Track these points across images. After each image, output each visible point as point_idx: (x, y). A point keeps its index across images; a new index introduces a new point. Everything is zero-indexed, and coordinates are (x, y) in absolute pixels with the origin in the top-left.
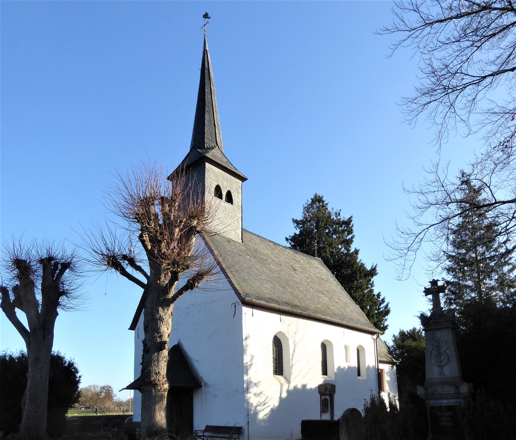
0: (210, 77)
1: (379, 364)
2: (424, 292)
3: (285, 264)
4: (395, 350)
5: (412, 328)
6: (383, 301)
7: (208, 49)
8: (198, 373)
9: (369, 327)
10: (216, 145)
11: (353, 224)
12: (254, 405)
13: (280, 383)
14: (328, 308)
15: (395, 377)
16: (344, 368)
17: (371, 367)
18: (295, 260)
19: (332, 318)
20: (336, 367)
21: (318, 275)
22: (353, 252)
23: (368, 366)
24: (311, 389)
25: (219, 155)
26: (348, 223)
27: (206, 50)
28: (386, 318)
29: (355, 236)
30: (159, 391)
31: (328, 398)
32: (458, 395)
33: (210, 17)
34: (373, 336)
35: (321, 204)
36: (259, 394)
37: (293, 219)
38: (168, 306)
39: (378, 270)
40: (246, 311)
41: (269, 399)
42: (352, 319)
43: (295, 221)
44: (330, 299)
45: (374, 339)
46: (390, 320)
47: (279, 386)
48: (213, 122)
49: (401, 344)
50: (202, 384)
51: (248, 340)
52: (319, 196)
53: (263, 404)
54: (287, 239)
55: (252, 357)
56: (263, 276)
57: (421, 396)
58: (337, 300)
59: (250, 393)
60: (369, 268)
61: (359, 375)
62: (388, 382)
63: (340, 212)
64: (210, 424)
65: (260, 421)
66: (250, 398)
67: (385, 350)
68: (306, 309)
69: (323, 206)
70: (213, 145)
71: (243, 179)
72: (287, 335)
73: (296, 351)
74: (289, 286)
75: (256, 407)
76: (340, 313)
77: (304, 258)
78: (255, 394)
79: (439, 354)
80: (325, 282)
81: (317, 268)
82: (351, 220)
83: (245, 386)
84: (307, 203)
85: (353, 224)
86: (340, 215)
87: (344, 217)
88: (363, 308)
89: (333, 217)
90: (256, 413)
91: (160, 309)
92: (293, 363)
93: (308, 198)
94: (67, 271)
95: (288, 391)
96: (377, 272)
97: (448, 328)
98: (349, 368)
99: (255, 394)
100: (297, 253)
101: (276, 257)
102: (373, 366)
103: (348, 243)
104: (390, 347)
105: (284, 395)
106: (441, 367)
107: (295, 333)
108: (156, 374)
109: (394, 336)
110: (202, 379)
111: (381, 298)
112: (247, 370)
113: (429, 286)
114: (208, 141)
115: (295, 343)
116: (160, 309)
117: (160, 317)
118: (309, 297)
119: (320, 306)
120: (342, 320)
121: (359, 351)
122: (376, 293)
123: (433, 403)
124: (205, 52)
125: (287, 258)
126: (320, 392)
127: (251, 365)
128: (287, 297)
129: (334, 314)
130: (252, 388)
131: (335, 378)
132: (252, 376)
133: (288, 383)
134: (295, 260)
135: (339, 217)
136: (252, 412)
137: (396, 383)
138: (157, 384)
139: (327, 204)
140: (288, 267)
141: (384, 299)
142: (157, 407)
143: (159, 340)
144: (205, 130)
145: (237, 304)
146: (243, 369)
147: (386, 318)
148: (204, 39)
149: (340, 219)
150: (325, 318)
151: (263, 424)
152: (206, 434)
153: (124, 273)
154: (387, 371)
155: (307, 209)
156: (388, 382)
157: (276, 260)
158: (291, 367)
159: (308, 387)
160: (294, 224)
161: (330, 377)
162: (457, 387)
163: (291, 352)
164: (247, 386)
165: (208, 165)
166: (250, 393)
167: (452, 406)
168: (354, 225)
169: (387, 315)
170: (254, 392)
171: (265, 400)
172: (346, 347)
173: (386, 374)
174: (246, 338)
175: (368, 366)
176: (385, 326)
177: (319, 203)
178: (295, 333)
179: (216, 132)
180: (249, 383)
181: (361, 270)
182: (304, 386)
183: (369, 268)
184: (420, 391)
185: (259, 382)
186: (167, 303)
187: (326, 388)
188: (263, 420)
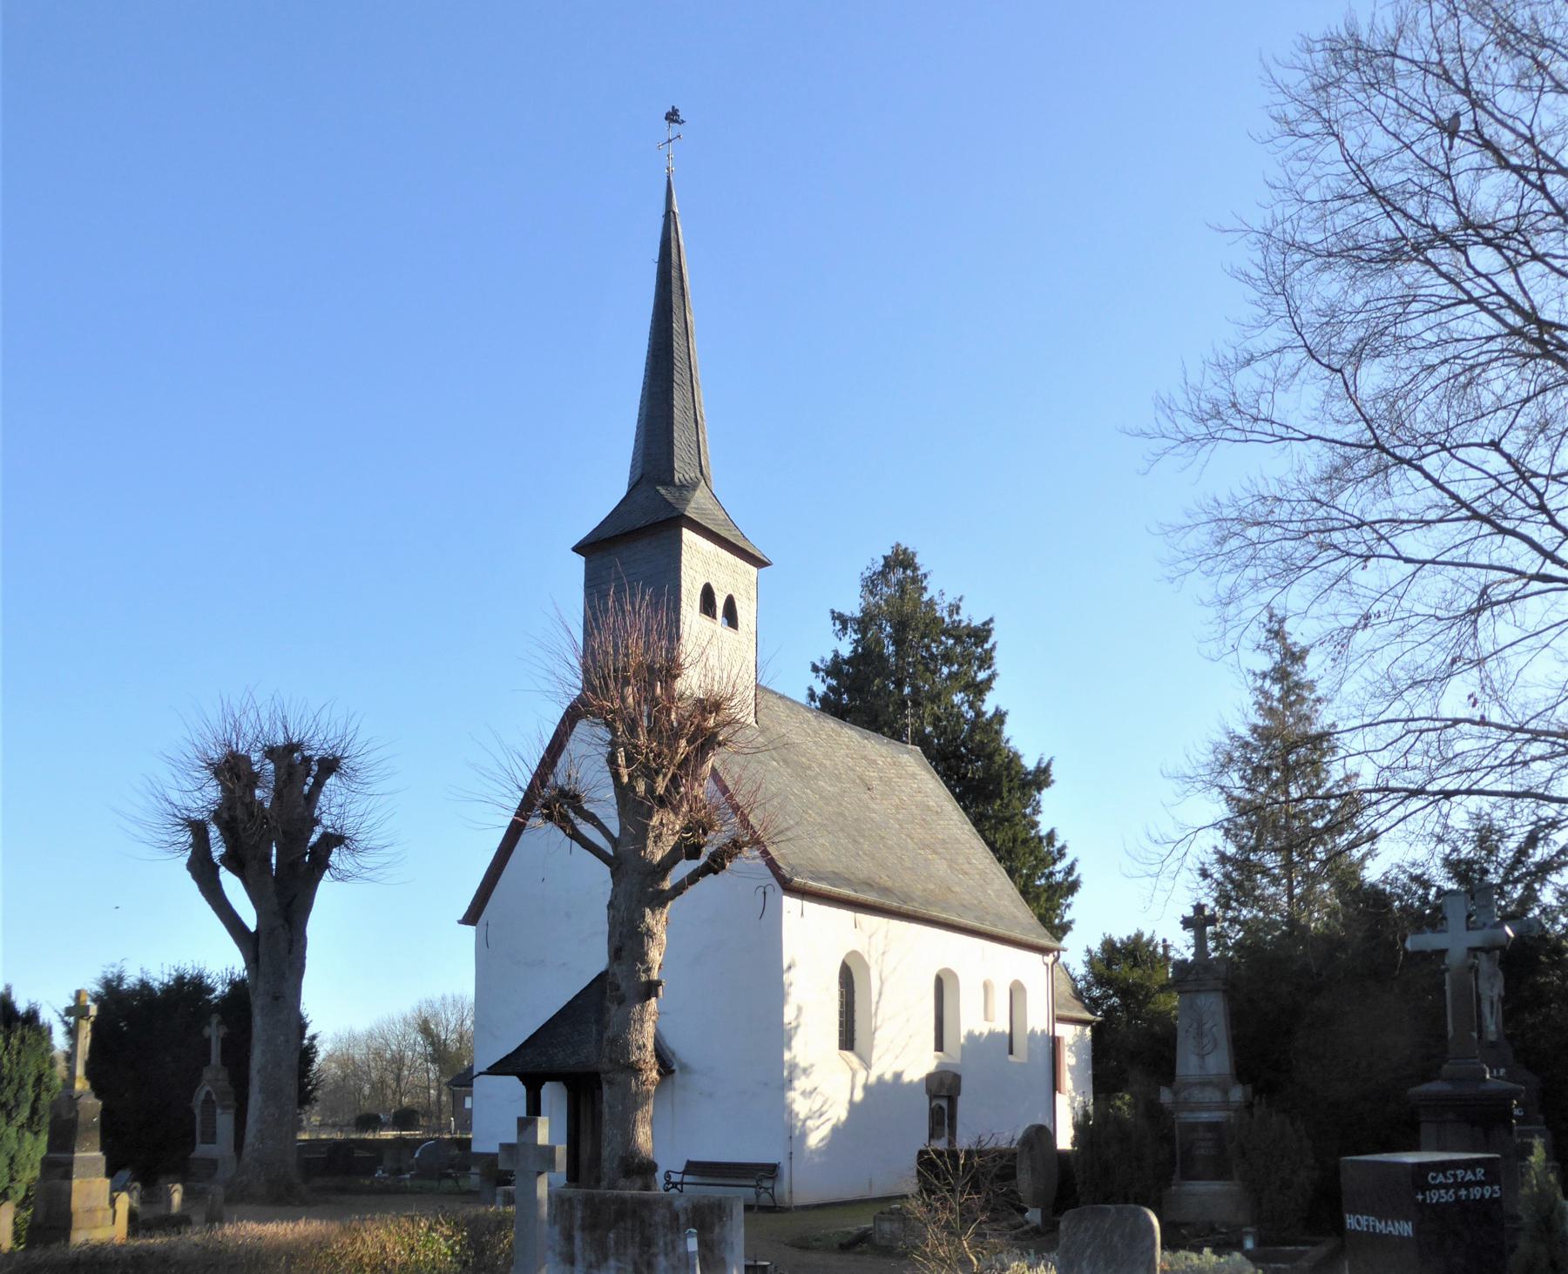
0: (683, 289)
1: (1056, 1025)
2: (1182, 922)
3: (847, 774)
4: (1089, 989)
5: (1132, 933)
6: (1061, 853)
7: (677, 211)
8: (664, 1041)
9: (1039, 936)
10: (699, 475)
11: (995, 643)
12: (802, 1116)
13: (852, 1069)
14: (950, 889)
15: (1087, 1056)
16: (981, 1034)
17: (1039, 1033)
18: (864, 758)
19: (961, 917)
20: (964, 1032)
21: (919, 798)
22: (991, 718)
23: (1032, 1031)
24: (911, 1082)
25: (709, 505)
26: (981, 634)
27: (674, 213)
28: (1068, 902)
29: (997, 675)
30: (643, 1083)
31: (944, 1104)
32: (1225, 1105)
33: (683, 122)
34: (1045, 958)
35: (909, 572)
36: (811, 1093)
37: (833, 612)
38: (663, 905)
39: (1055, 772)
40: (790, 904)
41: (829, 1103)
42: (999, 917)
43: (841, 620)
44: (952, 863)
45: (1047, 965)
46: (1077, 909)
47: (849, 1074)
48: (692, 412)
49: (1106, 973)
50: (675, 1067)
51: (793, 971)
52: (906, 549)
53: (818, 1114)
54: (815, 669)
55: (800, 1009)
56: (810, 816)
57: (1166, 1106)
58: (966, 867)
59: (794, 1090)
60: (1029, 763)
61: (1011, 1052)
62: (1071, 1069)
63: (961, 604)
64: (694, 1158)
65: (812, 1152)
66: (794, 1101)
67: (1065, 989)
68: (908, 898)
69: (915, 580)
70: (693, 475)
71: (758, 562)
72: (866, 958)
73: (883, 997)
74: (863, 836)
75: (805, 1121)
76: (976, 902)
77: (884, 750)
78: (803, 1093)
79: (1200, 1034)
80: (935, 818)
81: (913, 776)
82: (989, 631)
83: (785, 1073)
84: (870, 566)
85: (995, 643)
86: (960, 612)
87: (971, 615)
88: (1011, 872)
89: (942, 612)
90: (804, 1135)
91: (648, 911)
92: (878, 1024)
93: (874, 555)
94: (332, 781)
95: (866, 1088)
96: (1052, 778)
97: (1216, 990)
98: (992, 1034)
99: (803, 1093)
100: (866, 739)
101: (826, 755)
102: (1043, 1031)
103: (979, 690)
104: (1079, 978)
105: (859, 1095)
106: (1202, 1057)
107: (884, 953)
108: (639, 1048)
109: (1089, 951)
110: (674, 1054)
111: (1058, 844)
112: (790, 1039)
113: (1190, 913)
114: (682, 465)
115: (883, 977)
116: (648, 911)
117: (648, 929)
118: (908, 864)
119: (931, 886)
120: (982, 920)
121: (1016, 993)
122: (1044, 830)
123: (1188, 1117)
124: (669, 215)
125: (847, 756)
126: (929, 1091)
127: (797, 1027)
128: (864, 868)
129: (963, 906)
130: (799, 1078)
131: (962, 1059)
132: (799, 1051)
133: (866, 1069)
134: (864, 758)
135: (956, 618)
136: (797, 1132)
137: (1090, 1072)
138: (641, 1070)
139: (925, 576)
140: (854, 782)
141: (1064, 847)
142: (640, 1115)
143: (644, 978)
144: (675, 435)
145: (769, 890)
146: (780, 1036)
147: (1068, 902)
148: (666, 179)
149: (960, 621)
150: (946, 919)
151: (817, 1160)
152: (687, 1179)
153: (576, 836)
154: (1071, 1042)
155: (871, 584)
156: (1071, 1069)
157: (828, 763)
158: (874, 1033)
159: (906, 1078)
160: (834, 625)
161: (948, 1055)
162: (1226, 1092)
163: (875, 997)
164: (790, 1073)
165: (687, 535)
166: (794, 1090)
167: (1217, 1122)
168: (997, 646)
169: (1072, 895)
170: (802, 1089)
171: (822, 1106)
172: (987, 987)
173: (1067, 1049)
174: (790, 968)
175: (1032, 1031)
176: (1066, 923)
177: (905, 569)
178: (884, 953)
179: (698, 441)
180: (794, 1067)
181: (1013, 773)
182: (898, 1076)
183: (1029, 763)
184: (1166, 1096)
185: (812, 1066)
186: (660, 900)
187: (941, 1084)
188: (817, 1151)
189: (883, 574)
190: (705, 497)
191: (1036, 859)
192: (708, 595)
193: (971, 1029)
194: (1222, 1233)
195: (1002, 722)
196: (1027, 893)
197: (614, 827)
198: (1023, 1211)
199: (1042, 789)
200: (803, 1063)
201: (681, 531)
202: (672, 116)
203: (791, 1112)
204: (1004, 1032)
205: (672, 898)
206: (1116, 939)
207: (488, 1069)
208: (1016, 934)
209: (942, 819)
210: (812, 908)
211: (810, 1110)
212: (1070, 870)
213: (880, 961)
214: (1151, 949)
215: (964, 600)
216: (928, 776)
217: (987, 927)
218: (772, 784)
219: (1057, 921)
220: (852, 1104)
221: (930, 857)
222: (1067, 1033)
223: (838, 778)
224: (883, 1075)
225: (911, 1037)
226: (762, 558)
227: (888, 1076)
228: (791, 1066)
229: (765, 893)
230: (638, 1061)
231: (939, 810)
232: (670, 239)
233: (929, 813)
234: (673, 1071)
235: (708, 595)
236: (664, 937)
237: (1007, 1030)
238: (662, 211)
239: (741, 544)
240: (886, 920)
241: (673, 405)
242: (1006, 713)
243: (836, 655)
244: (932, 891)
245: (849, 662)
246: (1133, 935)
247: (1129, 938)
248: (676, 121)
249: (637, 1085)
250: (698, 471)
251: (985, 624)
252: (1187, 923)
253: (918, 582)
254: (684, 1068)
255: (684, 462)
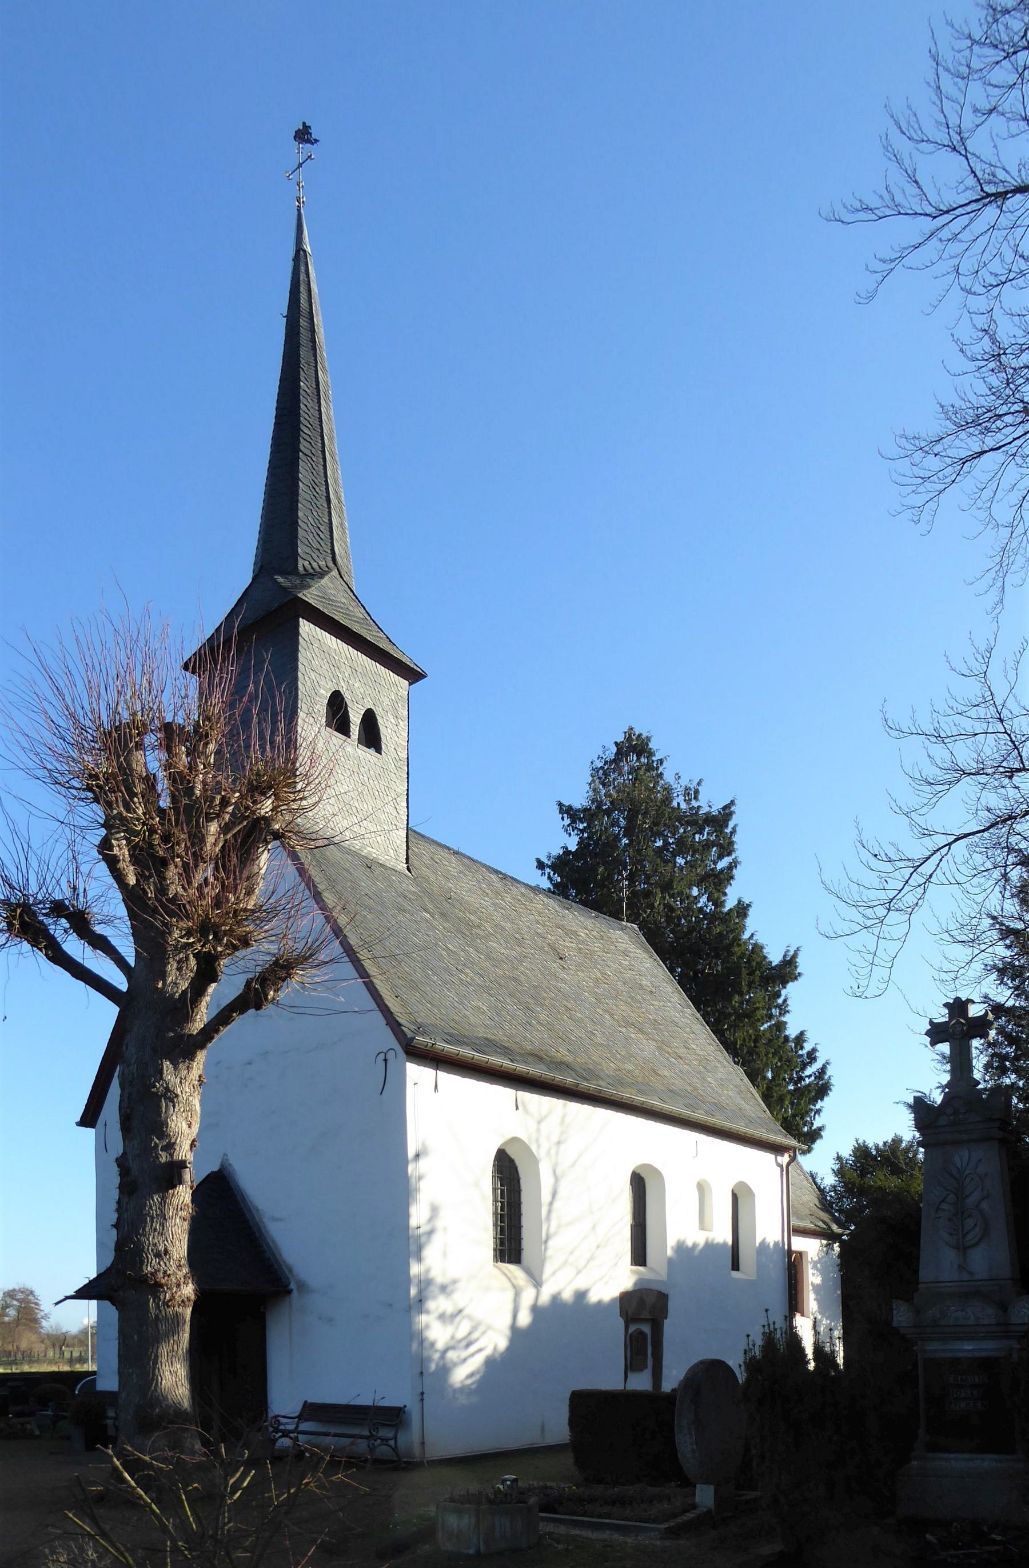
0: (314, 341)
6: (812, 1056)
7: (308, 249)
8: (281, 1255)
10: (331, 564)
12: (440, 1345)
13: (514, 1286)
15: (835, 1275)
16: (695, 1245)
19: (665, 1102)
20: (671, 1242)
21: (629, 975)
24: (600, 1303)
26: (721, 820)
27: (305, 251)
28: (818, 1107)
30: (166, 1304)
31: (646, 1329)
33: (316, 141)
34: (779, 1158)
38: (191, 1056)
39: (803, 965)
40: (416, 1074)
41: (481, 1329)
42: (720, 1107)
45: (781, 1166)
47: (510, 1294)
48: (323, 488)
49: (858, 1181)
50: (293, 1286)
52: (640, 735)
53: (464, 1343)
54: (541, 865)
55: (435, 1210)
56: (467, 975)
58: (682, 1051)
59: (428, 1312)
60: (775, 957)
62: (816, 1289)
63: (700, 788)
66: (427, 1326)
67: (810, 1199)
68: (591, 1074)
69: (649, 767)
70: (322, 563)
71: (412, 675)
74: (542, 1005)
76: (689, 1089)
77: (589, 923)
78: (442, 1317)
80: (648, 997)
81: (625, 953)
83: (413, 1291)
86: (700, 797)
87: (710, 802)
88: (753, 1076)
90: (445, 1370)
91: (167, 1064)
92: (552, 1230)
95: (535, 1309)
96: (799, 970)
98: (709, 1246)
99: (442, 1317)
100: (568, 909)
101: (507, 918)
102: (776, 1244)
103: (720, 881)
105: (525, 1319)
107: (559, 1143)
108: (158, 1255)
109: (839, 1158)
110: (291, 1271)
111: (808, 1047)
112: (420, 1248)
113: (941, 1016)
114: (308, 550)
115: (558, 1172)
116: (167, 1064)
117: (167, 1089)
118: (600, 1039)
119: (630, 1067)
120: (693, 1108)
122: (792, 1032)
123: (935, 1348)
124: (300, 256)
125: (538, 922)
127: (430, 1233)
128: (536, 1039)
129: (671, 1091)
130: (434, 1298)
135: (694, 804)
136: (433, 1367)
137: (839, 1292)
138: (161, 1286)
139: (661, 761)
140: (542, 948)
141: (814, 1050)
142: (164, 1350)
143: (164, 1157)
144: (300, 514)
145: (391, 1055)
147: (818, 1107)
148: (296, 212)
149: (699, 807)
150: (643, 1103)
154: (816, 1258)
155: (603, 774)
156: (816, 1289)
157: (508, 926)
158: (546, 1242)
159: (593, 1298)
161: (652, 1270)
163: (546, 1196)
164: (420, 1292)
165: (306, 628)
166: (428, 1312)
169: (822, 1100)
170: (441, 1310)
171: (470, 1334)
172: (702, 1189)
173: (810, 1266)
174: (417, 1156)
175: (763, 1243)
178: (559, 1143)
179: (331, 523)
180: (426, 1284)
183: (775, 957)
184: (901, 1316)
187: (642, 1302)
188: (463, 1389)
189: (616, 761)
190: (336, 589)
191: (780, 1060)
192: (337, 705)
193: (682, 1238)
194: (995, 1542)
195: (745, 915)
196: (771, 1097)
197: (128, 950)
198: (687, 1483)
199: (787, 982)
200: (438, 1275)
201: (297, 626)
202: (303, 135)
203: (422, 1341)
204: (725, 1244)
205: (202, 1047)
206: (871, 1144)
207: (76, 1292)
208: (741, 1127)
209: (657, 1000)
210: (449, 1080)
211: (453, 1337)
212: (823, 1071)
213: (553, 1152)
214: (910, 1155)
215: (703, 783)
216: (645, 955)
217: (700, 1116)
218: (415, 935)
219: (806, 1129)
220: (515, 1330)
221: (633, 1036)
222: (811, 1248)
223: (520, 943)
224: (559, 1293)
225: (598, 1247)
226: (412, 665)
227: (567, 1295)
228: (420, 1282)
229: (385, 1060)
230: (154, 1274)
231: (654, 990)
232: (299, 282)
233: (641, 992)
234: (290, 1292)
235: (337, 705)
236: (196, 1102)
237: (730, 1242)
238: (292, 254)
239: (383, 645)
240: (561, 1102)
241: (298, 479)
242: (749, 906)
243: (565, 848)
244: (629, 1071)
245: (575, 854)
246: (890, 1141)
247: (885, 1143)
248: (309, 141)
249: (158, 1307)
250: (329, 559)
251: (726, 807)
252: (937, 1033)
253: (653, 768)
254: (302, 1286)
255: (311, 546)
